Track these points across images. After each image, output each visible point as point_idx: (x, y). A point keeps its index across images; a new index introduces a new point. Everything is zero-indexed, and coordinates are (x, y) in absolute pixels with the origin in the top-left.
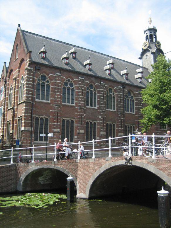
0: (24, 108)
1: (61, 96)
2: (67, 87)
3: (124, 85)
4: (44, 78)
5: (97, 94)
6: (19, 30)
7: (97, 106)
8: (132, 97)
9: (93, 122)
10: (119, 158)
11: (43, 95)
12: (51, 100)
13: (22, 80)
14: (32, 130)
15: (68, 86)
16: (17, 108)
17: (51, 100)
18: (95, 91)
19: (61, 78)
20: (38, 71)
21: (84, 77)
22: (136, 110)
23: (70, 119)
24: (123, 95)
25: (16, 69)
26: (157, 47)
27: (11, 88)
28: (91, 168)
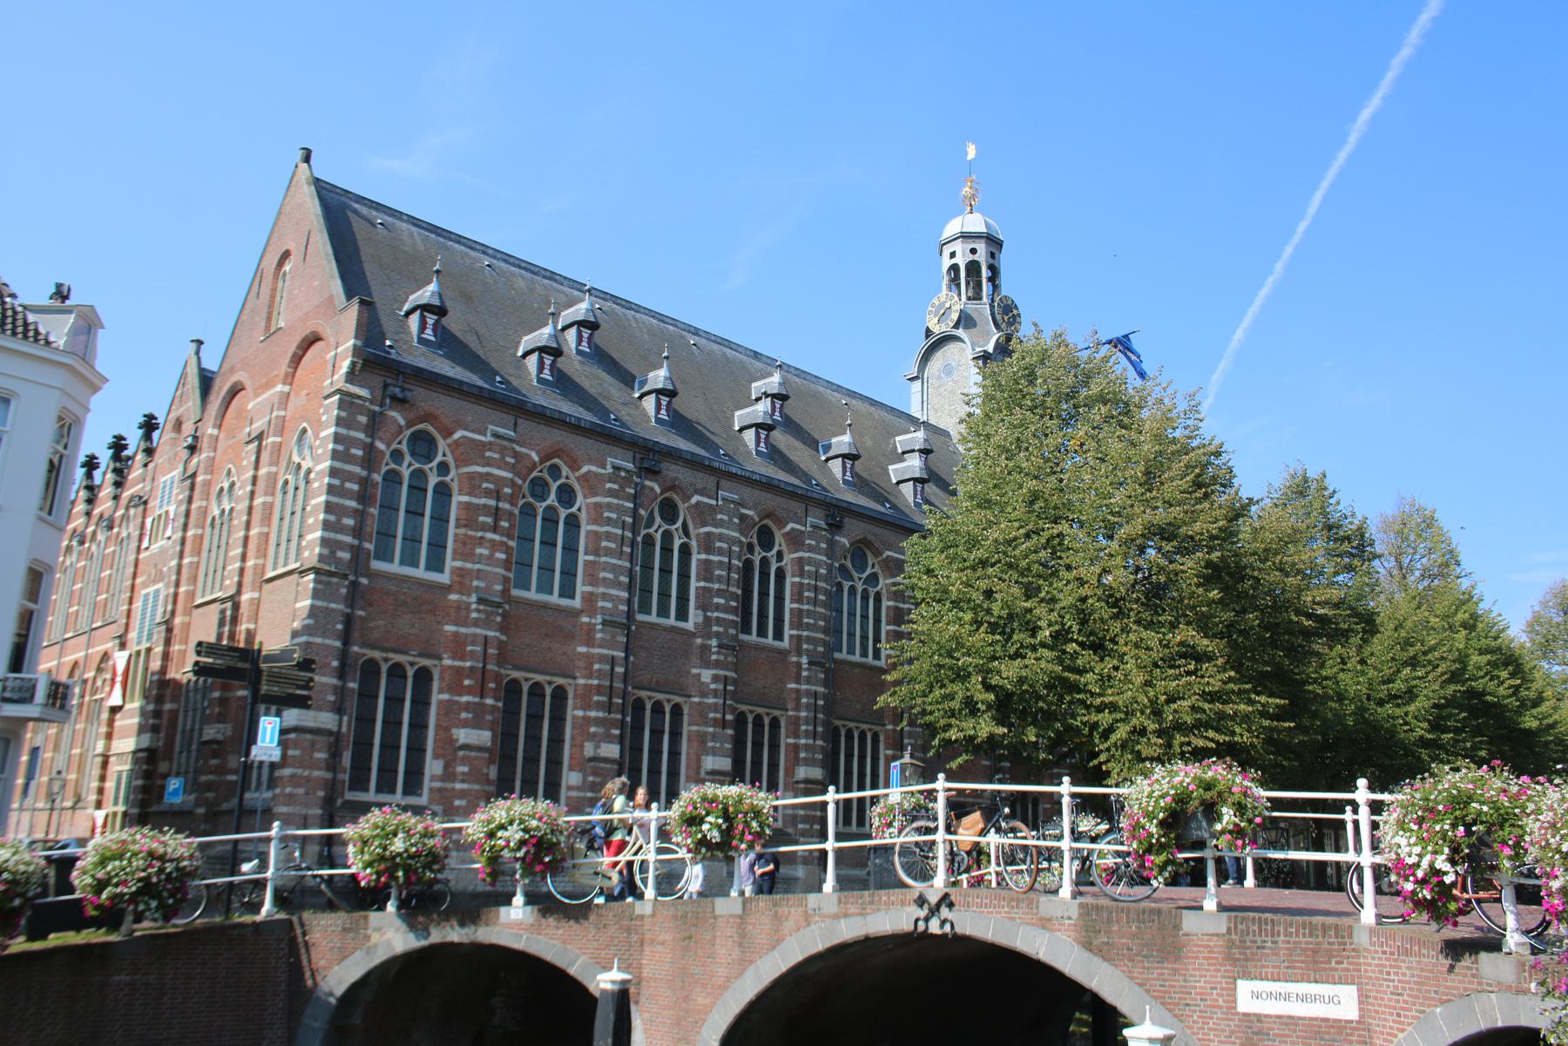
0: (309, 602)
1: (508, 550)
2: (541, 507)
4: (423, 446)
7: (694, 617)
10: (884, 895)
12: (455, 571)
13: (300, 453)
14: (344, 729)
15: (548, 502)
16: (259, 599)
17: (455, 571)
19: (516, 455)
20: (656, 481)
24: (830, 567)
25: (269, 385)
26: (1003, 326)
27: (226, 485)
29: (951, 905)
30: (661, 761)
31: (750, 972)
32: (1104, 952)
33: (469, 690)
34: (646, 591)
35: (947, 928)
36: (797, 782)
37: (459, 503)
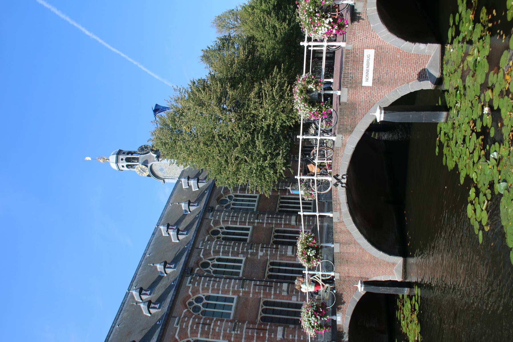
3: (208, 209)
5: (220, 255)
7: (241, 257)
8: (230, 197)
9: (269, 267)
11: (224, 307)
15: (201, 306)
19: (184, 317)
21: (174, 317)
23: (260, 307)
24: (226, 212)
29: (337, 175)
31: (358, 241)
32: (353, 128)
33: (264, 334)
35: (345, 177)
36: (296, 224)
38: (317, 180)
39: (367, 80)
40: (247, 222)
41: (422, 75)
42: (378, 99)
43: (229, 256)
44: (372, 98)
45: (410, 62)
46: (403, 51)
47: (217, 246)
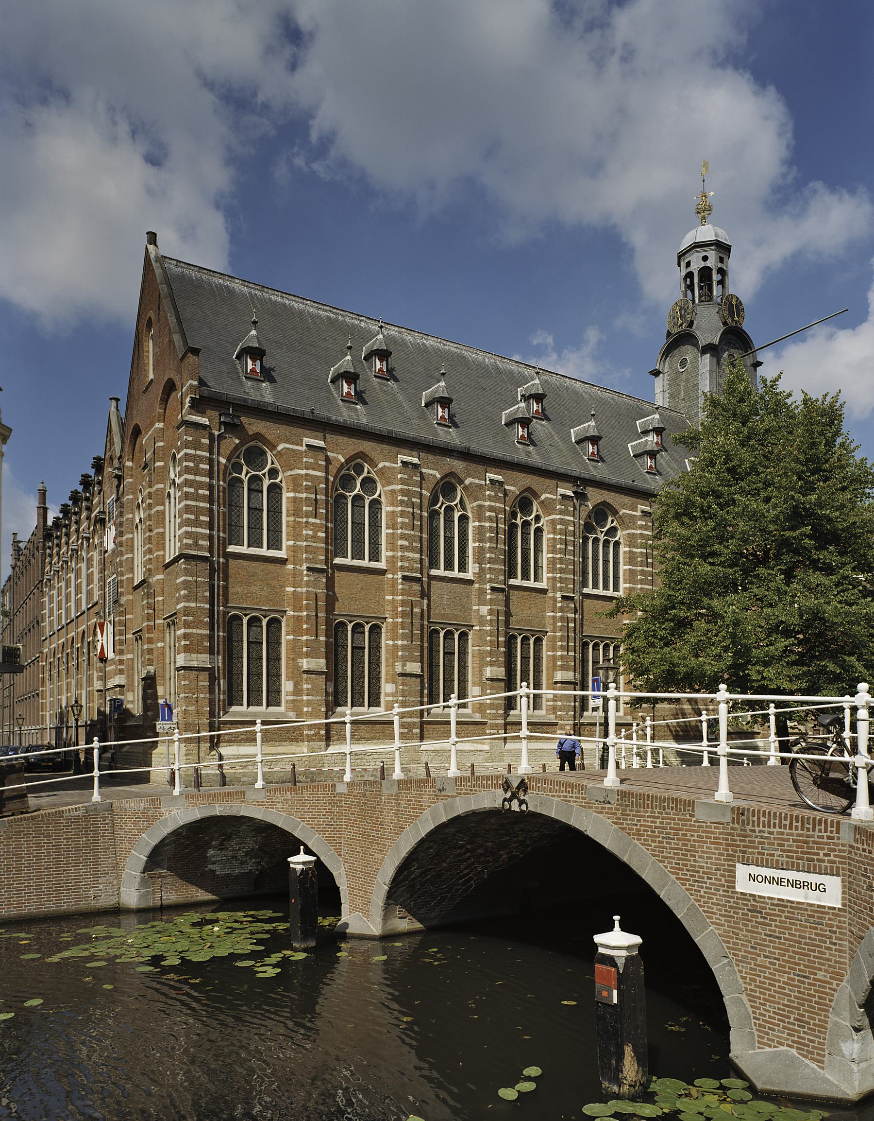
6: (152, 257)
7: (472, 569)
12: (288, 547)
15: (356, 492)
17: (288, 547)
18: (464, 509)
21: (325, 438)
22: (625, 582)
28: (388, 817)
30: (453, 673)
33: (307, 632)
34: (584, 573)
35: (524, 807)
36: (556, 683)
37: (288, 498)
38: (768, 714)
39: (753, 878)
40: (555, 575)
41: (768, 1034)
42: (702, 903)
43: (474, 541)
44: (706, 888)
45: (803, 1005)
46: (835, 990)
47: (493, 514)
